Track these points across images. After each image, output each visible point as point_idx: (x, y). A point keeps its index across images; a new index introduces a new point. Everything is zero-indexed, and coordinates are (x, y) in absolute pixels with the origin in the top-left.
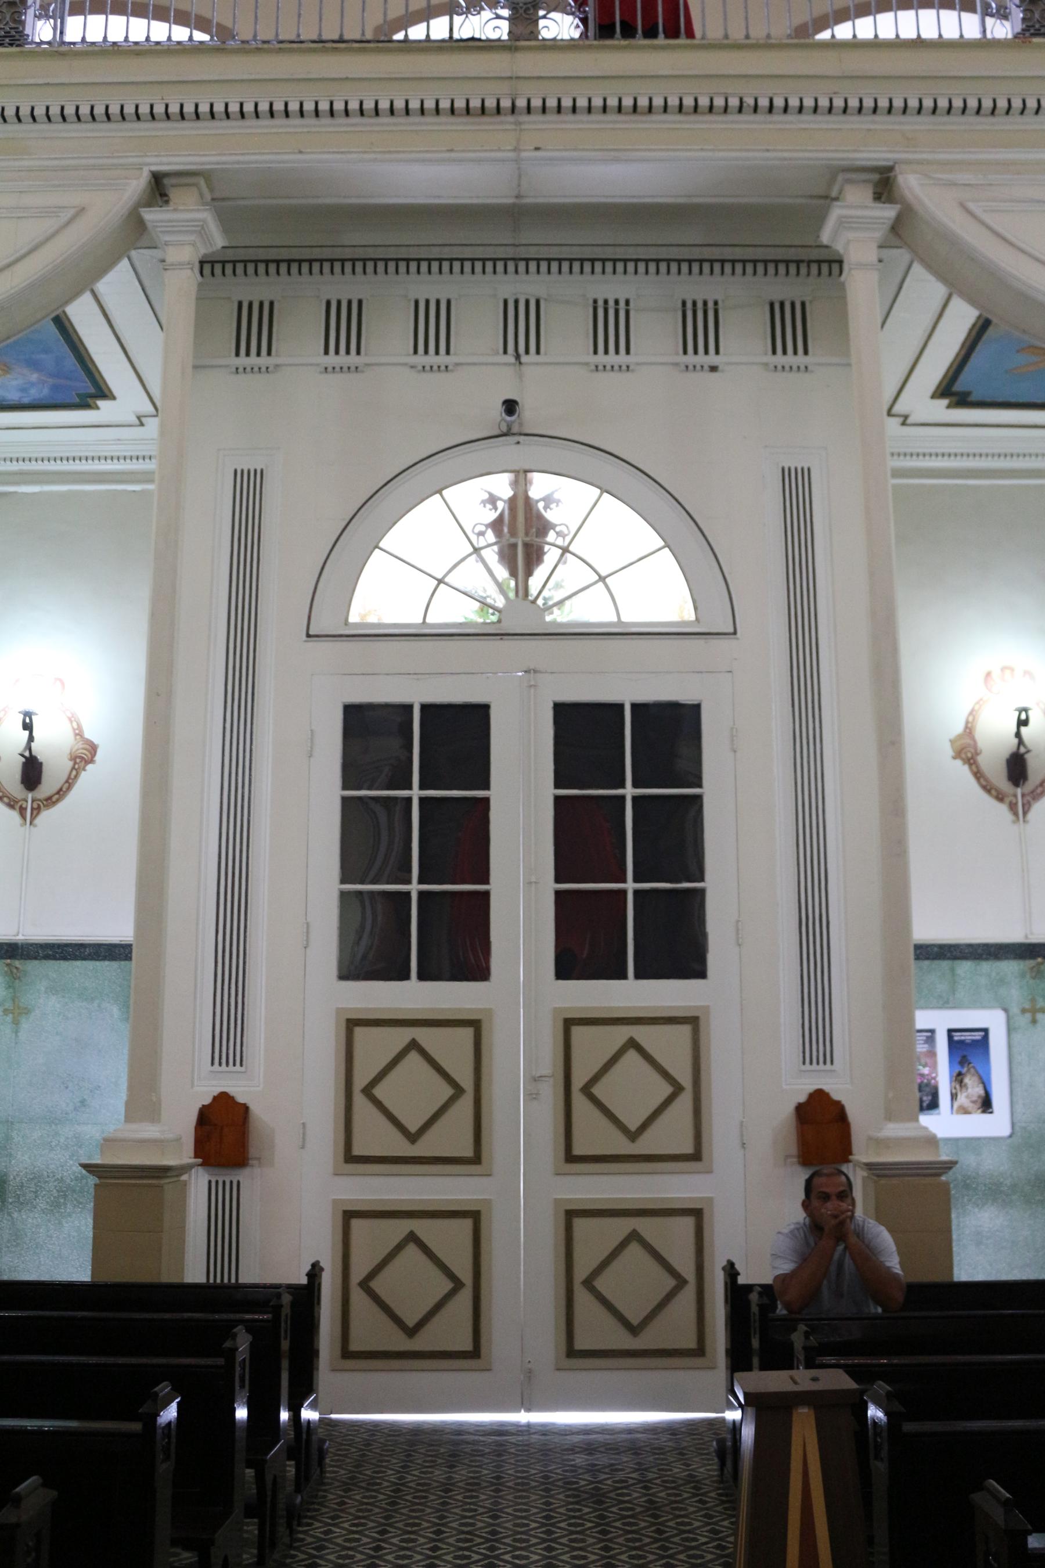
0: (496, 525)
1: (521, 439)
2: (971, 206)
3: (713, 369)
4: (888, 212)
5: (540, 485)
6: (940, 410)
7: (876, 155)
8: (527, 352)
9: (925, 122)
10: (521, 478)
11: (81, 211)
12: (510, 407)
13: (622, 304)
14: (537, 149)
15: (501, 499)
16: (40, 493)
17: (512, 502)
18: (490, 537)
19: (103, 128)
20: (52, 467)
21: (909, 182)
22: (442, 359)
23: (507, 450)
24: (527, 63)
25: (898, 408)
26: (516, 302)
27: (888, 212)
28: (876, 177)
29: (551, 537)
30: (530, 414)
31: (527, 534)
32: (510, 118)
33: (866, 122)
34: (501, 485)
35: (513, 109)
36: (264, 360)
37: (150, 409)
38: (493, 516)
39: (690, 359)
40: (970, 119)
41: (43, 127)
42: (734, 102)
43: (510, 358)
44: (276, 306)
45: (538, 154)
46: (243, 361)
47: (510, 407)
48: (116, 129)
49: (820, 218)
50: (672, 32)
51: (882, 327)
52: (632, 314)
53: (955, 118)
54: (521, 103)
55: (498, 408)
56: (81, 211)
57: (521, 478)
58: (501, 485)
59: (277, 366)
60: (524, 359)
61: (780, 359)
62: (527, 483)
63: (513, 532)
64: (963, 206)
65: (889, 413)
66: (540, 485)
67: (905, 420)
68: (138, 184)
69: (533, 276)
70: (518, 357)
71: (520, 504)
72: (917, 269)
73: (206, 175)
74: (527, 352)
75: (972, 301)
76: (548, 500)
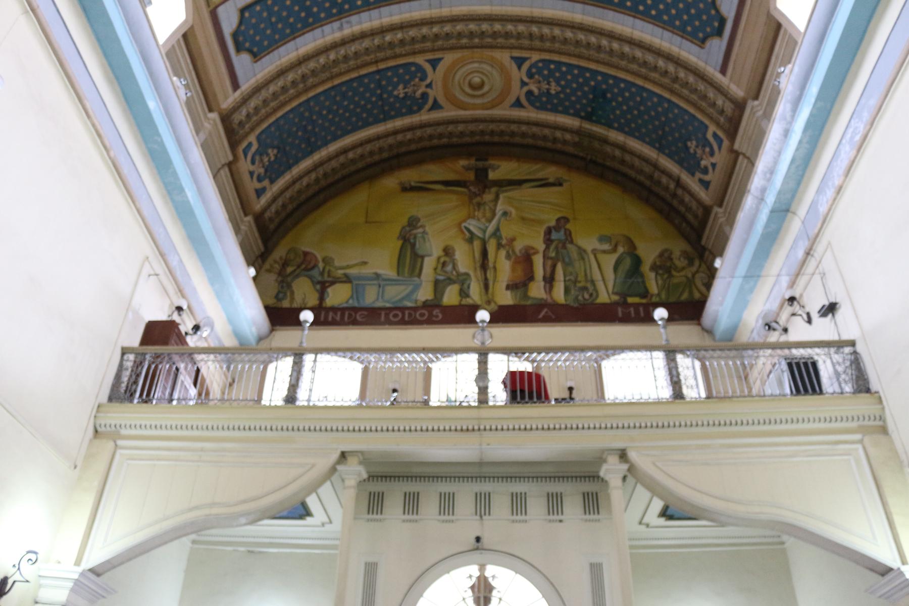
0: (472, 588)
1: (483, 551)
2: (658, 464)
3: (561, 521)
4: (625, 467)
5: (491, 571)
6: (662, 521)
7: (620, 445)
8: (485, 514)
9: (637, 431)
10: (482, 568)
11: (313, 466)
12: (478, 539)
13: (523, 495)
14: (488, 445)
15: (495, 303)
16: (278, 553)
17: (479, 578)
18: (470, 593)
19: (324, 434)
20: (282, 541)
21: (632, 455)
22: (451, 517)
23: (476, 555)
24: (484, 413)
25: (645, 521)
26: (481, 494)
27: (625, 467)
28: (619, 452)
29: (494, 593)
30: (485, 541)
31: (485, 592)
32: (478, 433)
33: (614, 432)
34: (474, 570)
35: (479, 429)
36: (379, 516)
37: (327, 520)
38: (471, 584)
39: (551, 517)
40: (654, 430)
41: (302, 433)
42: (563, 426)
43: (478, 517)
44: (385, 494)
45: (489, 447)
46: (371, 516)
47: (478, 539)
48: (329, 434)
49: (600, 466)
50: (539, 397)
51: (626, 510)
52: (527, 498)
53: (649, 430)
54: (482, 427)
55: (473, 540)
56: (313, 466)
57: (482, 568)
58: (474, 570)
59: (384, 519)
60: (484, 517)
61: (588, 517)
62: (485, 569)
63: (479, 591)
64: (654, 464)
65: (640, 523)
66: (491, 571)
67: (647, 526)
68: (336, 456)
69: (487, 483)
70: (481, 516)
71: (482, 580)
72: (639, 487)
73: (362, 453)
74: (485, 514)
75: (661, 498)
76: (493, 577)
